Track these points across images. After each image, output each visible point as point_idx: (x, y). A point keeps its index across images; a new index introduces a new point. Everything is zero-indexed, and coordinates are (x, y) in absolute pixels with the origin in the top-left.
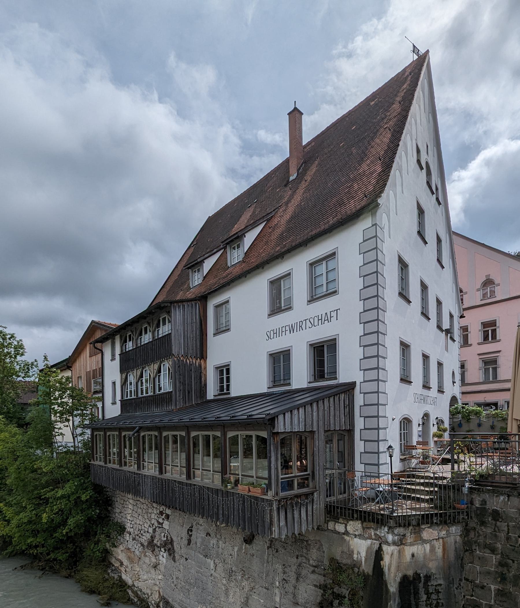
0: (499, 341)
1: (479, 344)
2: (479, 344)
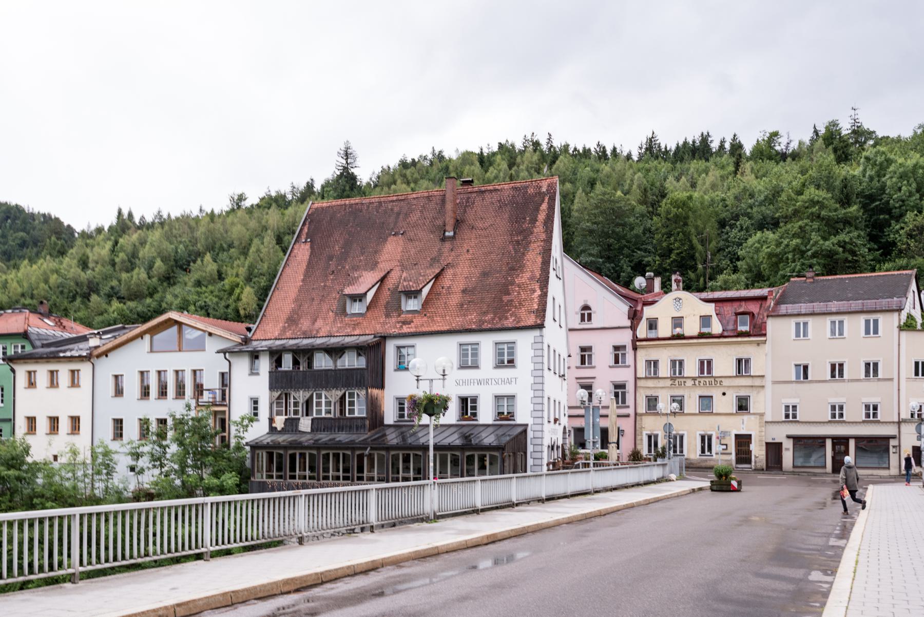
0: (594, 367)
1: (577, 368)
2: (577, 368)
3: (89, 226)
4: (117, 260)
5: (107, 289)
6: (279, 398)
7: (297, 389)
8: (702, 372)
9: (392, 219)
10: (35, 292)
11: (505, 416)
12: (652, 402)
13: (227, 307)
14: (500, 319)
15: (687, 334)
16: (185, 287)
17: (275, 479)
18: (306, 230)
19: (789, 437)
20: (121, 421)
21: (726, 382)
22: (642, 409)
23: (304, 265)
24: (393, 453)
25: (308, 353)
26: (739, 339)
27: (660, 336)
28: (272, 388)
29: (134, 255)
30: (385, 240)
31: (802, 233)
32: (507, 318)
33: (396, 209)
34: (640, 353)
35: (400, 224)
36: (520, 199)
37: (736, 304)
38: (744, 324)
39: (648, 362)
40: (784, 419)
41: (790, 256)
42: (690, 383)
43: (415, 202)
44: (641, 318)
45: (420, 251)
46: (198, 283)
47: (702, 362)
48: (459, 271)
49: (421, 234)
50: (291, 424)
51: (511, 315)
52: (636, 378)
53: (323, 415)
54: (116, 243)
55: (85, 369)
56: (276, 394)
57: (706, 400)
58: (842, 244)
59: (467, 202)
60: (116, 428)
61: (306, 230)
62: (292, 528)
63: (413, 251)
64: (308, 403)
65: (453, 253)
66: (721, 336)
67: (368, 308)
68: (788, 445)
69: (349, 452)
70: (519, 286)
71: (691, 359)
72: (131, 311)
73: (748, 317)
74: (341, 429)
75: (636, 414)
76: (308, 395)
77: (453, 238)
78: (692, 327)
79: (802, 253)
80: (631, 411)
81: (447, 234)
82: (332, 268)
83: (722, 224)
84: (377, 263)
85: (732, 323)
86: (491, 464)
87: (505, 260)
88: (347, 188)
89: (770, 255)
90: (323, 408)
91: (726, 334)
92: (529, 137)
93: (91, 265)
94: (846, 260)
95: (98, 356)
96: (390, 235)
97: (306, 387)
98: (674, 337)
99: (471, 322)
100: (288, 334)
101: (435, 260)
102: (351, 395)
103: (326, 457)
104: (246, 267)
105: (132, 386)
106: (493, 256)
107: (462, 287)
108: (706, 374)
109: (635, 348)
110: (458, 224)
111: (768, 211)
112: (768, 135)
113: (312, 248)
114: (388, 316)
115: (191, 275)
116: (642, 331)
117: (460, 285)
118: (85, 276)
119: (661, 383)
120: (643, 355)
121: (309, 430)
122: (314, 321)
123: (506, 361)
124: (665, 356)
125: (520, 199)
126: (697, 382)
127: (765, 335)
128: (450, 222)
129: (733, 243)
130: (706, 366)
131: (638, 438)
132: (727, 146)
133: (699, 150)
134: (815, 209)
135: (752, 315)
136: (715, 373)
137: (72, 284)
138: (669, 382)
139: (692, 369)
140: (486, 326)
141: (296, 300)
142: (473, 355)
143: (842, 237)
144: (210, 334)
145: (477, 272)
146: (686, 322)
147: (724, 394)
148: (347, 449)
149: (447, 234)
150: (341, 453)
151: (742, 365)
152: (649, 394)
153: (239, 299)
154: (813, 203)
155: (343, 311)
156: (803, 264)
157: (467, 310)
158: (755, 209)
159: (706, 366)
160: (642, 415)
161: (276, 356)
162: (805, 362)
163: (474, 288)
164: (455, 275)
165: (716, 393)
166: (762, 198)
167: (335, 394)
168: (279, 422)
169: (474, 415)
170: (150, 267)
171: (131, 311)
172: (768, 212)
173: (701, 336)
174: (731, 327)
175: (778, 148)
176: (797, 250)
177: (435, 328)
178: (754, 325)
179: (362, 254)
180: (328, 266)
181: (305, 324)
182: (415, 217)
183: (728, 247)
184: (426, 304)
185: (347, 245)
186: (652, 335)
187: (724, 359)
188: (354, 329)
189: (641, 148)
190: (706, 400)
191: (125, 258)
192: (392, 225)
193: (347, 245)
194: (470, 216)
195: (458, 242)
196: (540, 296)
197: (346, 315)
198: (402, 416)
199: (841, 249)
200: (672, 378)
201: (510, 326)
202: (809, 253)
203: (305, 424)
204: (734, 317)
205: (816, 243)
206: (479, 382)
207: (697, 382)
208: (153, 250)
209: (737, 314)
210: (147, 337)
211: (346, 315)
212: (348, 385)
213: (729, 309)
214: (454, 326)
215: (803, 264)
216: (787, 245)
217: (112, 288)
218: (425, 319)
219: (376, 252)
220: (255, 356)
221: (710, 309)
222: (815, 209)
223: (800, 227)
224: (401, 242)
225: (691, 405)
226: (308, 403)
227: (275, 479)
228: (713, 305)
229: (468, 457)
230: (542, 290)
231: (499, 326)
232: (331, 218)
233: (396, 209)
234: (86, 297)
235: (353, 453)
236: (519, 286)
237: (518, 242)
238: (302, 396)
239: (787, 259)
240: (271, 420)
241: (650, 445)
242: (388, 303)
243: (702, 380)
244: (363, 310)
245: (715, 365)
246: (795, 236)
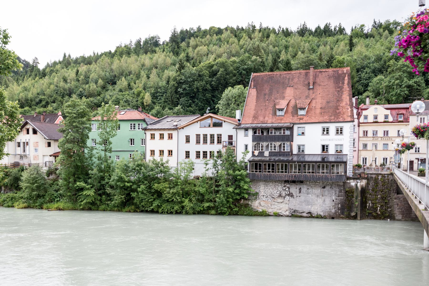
3: (51, 61)
4: (80, 79)
5: (78, 92)
6: (256, 144)
7: (263, 141)
8: (384, 135)
9: (287, 81)
10: (45, 93)
11: (339, 152)
12: (365, 146)
13: (137, 101)
14: (337, 119)
15: (379, 121)
16: (112, 93)
18: (253, 84)
19: (416, 159)
20: (189, 152)
21: (393, 139)
22: (361, 148)
23: (255, 97)
24: (304, 164)
25: (268, 129)
26: (399, 123)
27: (369, 122)
28: (253, 141)
29: (87, 77)
30: (286, 89)
31: (400, 78)
32: (339, 118)
33: (288, 77)
34: (360, 127)
35: (290, 83)
36: (336, 75)
37: (397, 110)
38: (401, 118)
41: (395, 87)
42: (380, 139)
43: (295, 75)
44: (361, 115)
45: (301, 93)
46: (121, 91)
47: (385, 132)
48: (317, 101)
49: (300, 87)
50: (261, 154)
51: (341, 117)
52: (359, 137)
53: (273, 151)
54: (78, 71)
55: (174, 133)
56: (255, 143)
57: (386, 145)
58: (416, 82)
59: (316, 75)
60: (186, 154)
61: (253, 84)
63: (298, 93)
64: (267, 146)
65: (314, 94)
66: (392, 122)
67: (285, 113)
68: (416, 161)
69: (287, 163)
70: (342, 107)
71: (380, 130)
72: (91, 102)
73: (402, 115)
74: (280, 155)
75: (358, 150)
76: (267, 144)
77: (313, 89)
78: (381, 119)
79: (401, 86)
80: (357, 149)
81: (310, 87)
82: (267, 98)
83: (358, 71)
84: (284, 97)
85: (396, 117)
86: (326, 167)
87: (335, 97)
88: (176, 47)
89: (387, 86)
90: (273, 148)
91: (394, 121)
92: (251, 24)
93: (68, 81)
94: (417, 89)
95: (179, 129)
96: (287, 86)
97: (267, 141)
98: (374, 122)
99: (326, 119)
100: (255, 122)
101: (307, 97)
102: (284, 144)
103: (265, 165)
104: (143, 84)
105: (193, 139)
106: (330, 96)
107: (320, 107)
109: (359, 126)
110: (314, 83)
111: (377, 65)
112: (360, 26)
113: (257, 90)
114: (293, 116)
115: (116, 86)
116: (362, 120)
117: (319, 106)
118: (67, 86)
119: (369, 139)
120: (362, 129)
121: (268, 156)
122: (264, 118)
123: (339, 131)
124: (370, 129)
125: (336, 75)
127: (409, 122)
128: (311, 83)
129: (364, 79)
130: (386, 133)
131: (359, 159)
132: (337, 29)
133: (325, 32)
134: (405, 68)
135: (403, 114)
136: (389, 135)
137: (62, 89)
138: (372, 139)
139: (380, 134)
140: (332, 121)
141: (255, 110)
142: (341, 130)
143: (415, 80)
144: (225, 121)
145: (325, 101)
146: (378, 117)
148: (286, 162)
149: (310, 87)
150: (271, 163)
152: (364, 143)
153: (143, 98)
154: (404, 66)
155: (275, 114)
156: (401, 90)
157: (324, 115)
158: (371, 65)
159: (386, 133)
160: (361, 150)
161: (255, 130)
163: (325, 107)
164: (316, 102)
165: (390, 143)
166: (373, 59)
167: (278, 144)
168: (256, 153)
169: (327, 151)
170: (96, 83)
171: (91, 102)
172: (377, 66)
173: (385, 122)
174: (395, 119)
175: (364, 32)
176: (397, 85)
177: (313, 121)
178: (404, 119)
179: (278, 93)
180: (265, 98)
181: (261, 119)
182: (296, 80)
183: (361, 81)
184: (307, 112)
185: (271, 90)
186: (365, 121)
187: (393, 130)
188: (281, 121)
189: (298, 29)
190: (386, 145)
191: (83, 78)
192: (287, 83)
193: (271, 90)
194: (318, 80)
195: (315, 90)
196: (351, 111)
197: (277, 116)
198: (299, 151)
199: (416, 85)
200: (373, 137)
201: (342, 121)
202: (403, 86)
203: (267, 154)
204: (396, 115)
205: (406, 82)
206: (329, 140)
208: (96, 74)
209: (398, 114)
210: (199, 122)
211: (277, 116)
212: (283, 140)
213: (394, 112)
214: (320, 121)
215: (401, 90)
216: (394, 83)
217: (81, 92)
218: (308, 118)
219: (283, 93)
220: (246, 129)
221: (388, 112)
222: (405, 68)
223: (399, 75)
224: (292, 89)
225: (380, 147)
226: (267, 146)
229: (304, 165)
230: (351, 109)
231: (337, 121)
232: (262, 79)
233: (288, 77)
234: (70, 95)
235: (316, 164)
236: (342, 107)
237: (338, 91)
238: (265, 144)
239: (394, 88)
240: (253, 152)
241: (363, 162)
242: (292, 112)
243: (384, 138)
244: (283, 114)
245: (389, 133)
246: (397, 79)
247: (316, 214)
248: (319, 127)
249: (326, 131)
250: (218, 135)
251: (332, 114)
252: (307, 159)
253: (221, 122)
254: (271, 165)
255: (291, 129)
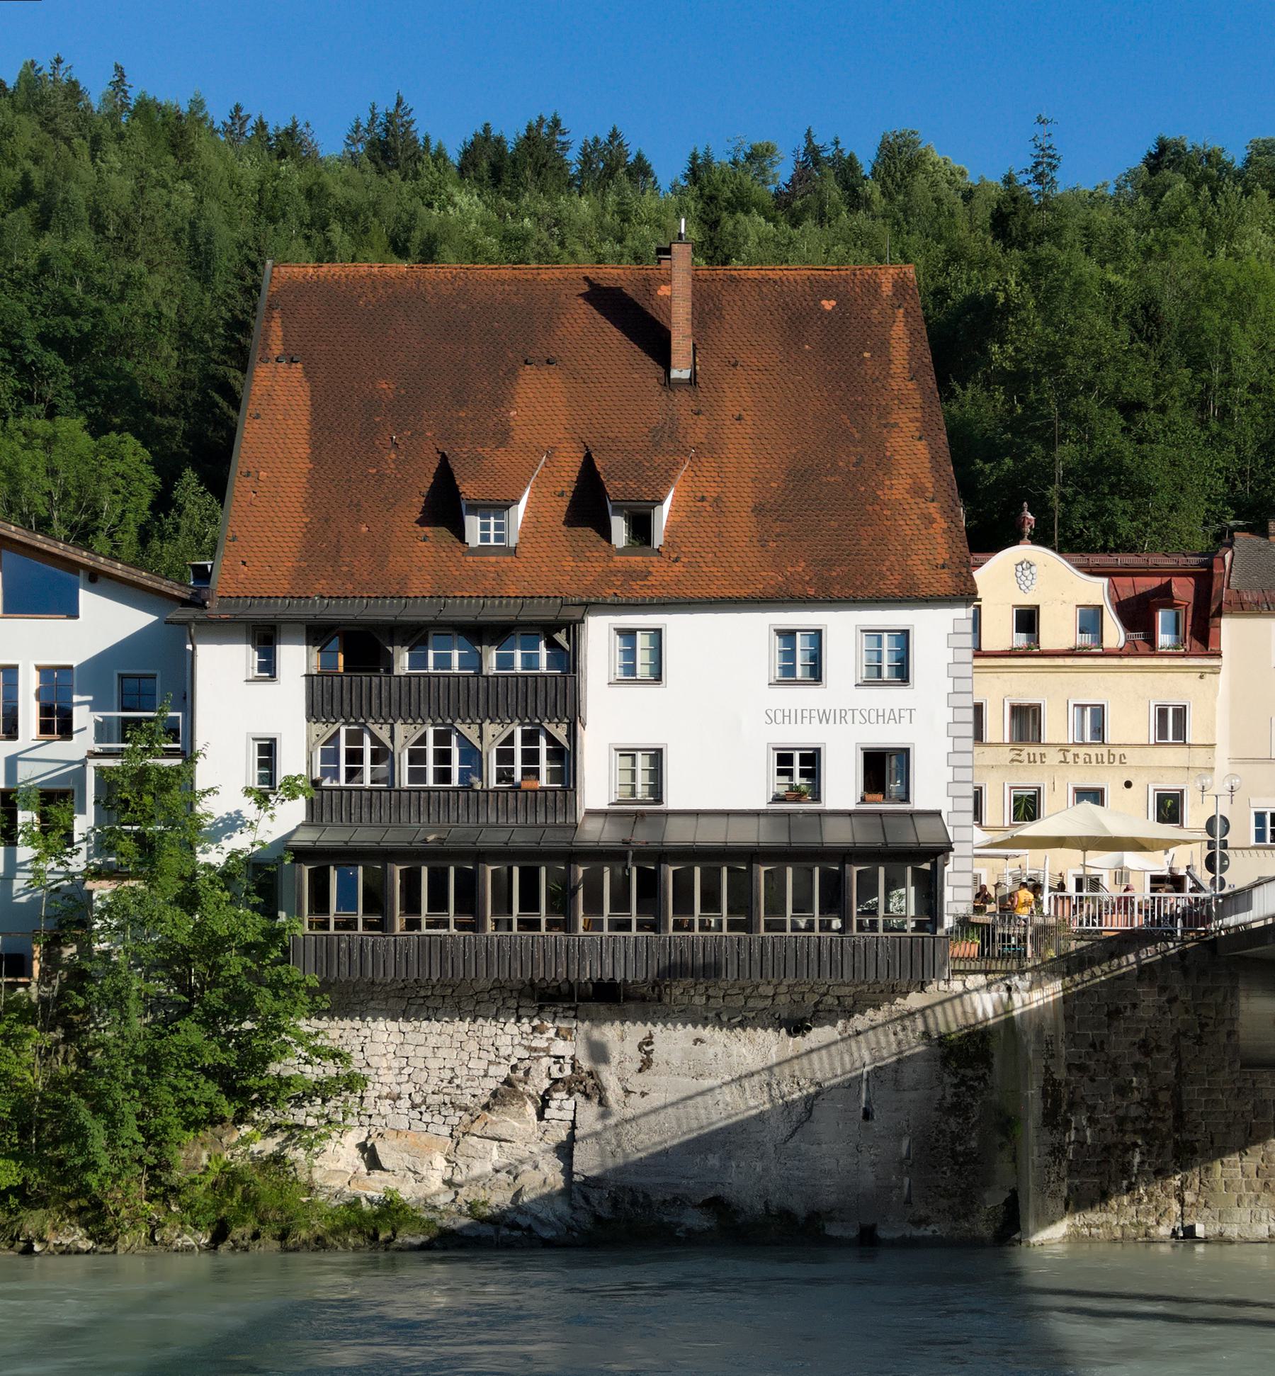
7: (389, 717)
17: (634, 932)
21: (1133, 756)
28: (315, 711)
30: (512, 373)
39: (66, 731)
40: (1253, 842)
42: (1054, 756)
62: (951, 1018)
97: (413, 715)
108: (1170, 740)
126: (1070, 757)
147: (1128, 785)
151: (1171, 724)
162: (652, 741)
206: (824, 717)
207: (1070, 757)
220: (265, 639)
227: (634, 932)
228: (1105, 581)
247: (759, 1206)
248: (753, 632)
249: (803, 663)
250: (45, 672)
251: (814, 558)
252: (678, 834)
253: (1156, 582)
254: (454, 876)
255: (559, 631)
